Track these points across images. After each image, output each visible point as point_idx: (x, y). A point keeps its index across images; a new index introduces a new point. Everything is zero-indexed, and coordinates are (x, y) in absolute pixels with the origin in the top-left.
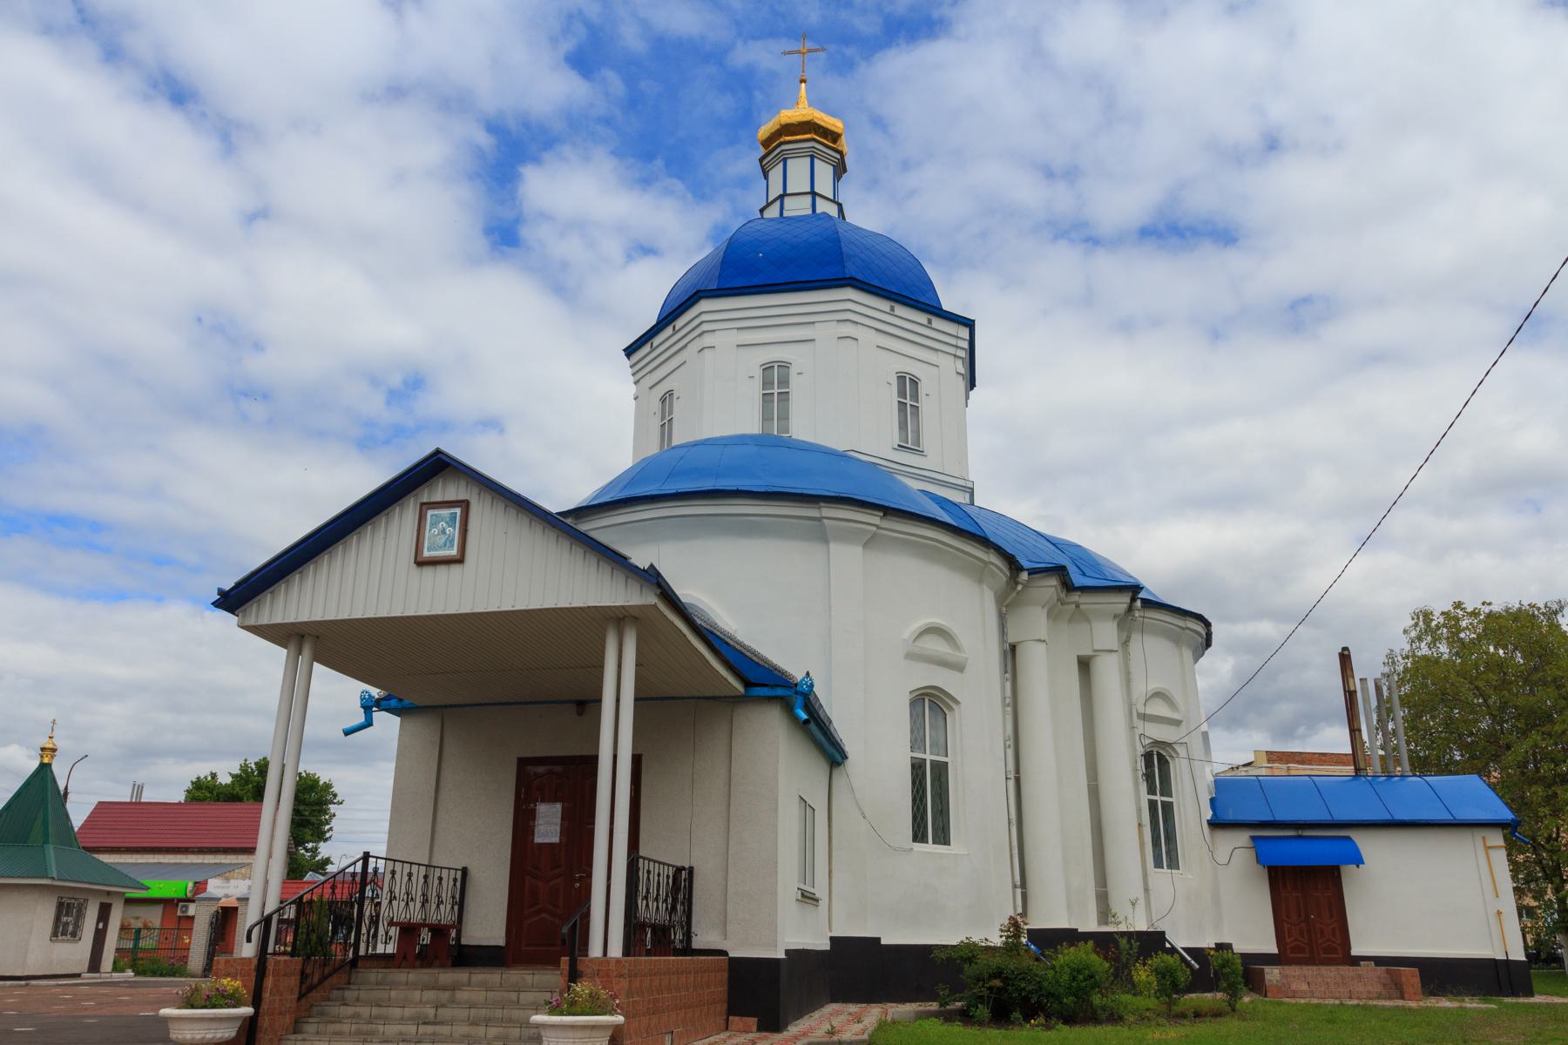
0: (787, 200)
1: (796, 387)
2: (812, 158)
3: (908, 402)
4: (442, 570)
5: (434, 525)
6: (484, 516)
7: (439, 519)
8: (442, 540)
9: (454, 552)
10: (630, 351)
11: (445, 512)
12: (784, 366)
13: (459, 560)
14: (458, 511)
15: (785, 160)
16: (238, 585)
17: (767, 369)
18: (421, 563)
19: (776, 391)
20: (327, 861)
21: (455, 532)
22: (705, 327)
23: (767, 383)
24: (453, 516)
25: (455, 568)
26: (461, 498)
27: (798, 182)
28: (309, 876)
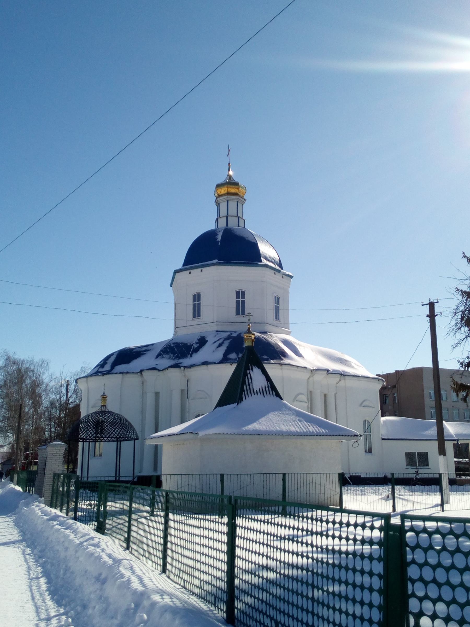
2: (228, 202)
3: (241, 300)
10: (171, 285)
12: (199, 295)
15: (219, 204)
17: (195, 296)
19: (241, 300)
23: (195, 301)
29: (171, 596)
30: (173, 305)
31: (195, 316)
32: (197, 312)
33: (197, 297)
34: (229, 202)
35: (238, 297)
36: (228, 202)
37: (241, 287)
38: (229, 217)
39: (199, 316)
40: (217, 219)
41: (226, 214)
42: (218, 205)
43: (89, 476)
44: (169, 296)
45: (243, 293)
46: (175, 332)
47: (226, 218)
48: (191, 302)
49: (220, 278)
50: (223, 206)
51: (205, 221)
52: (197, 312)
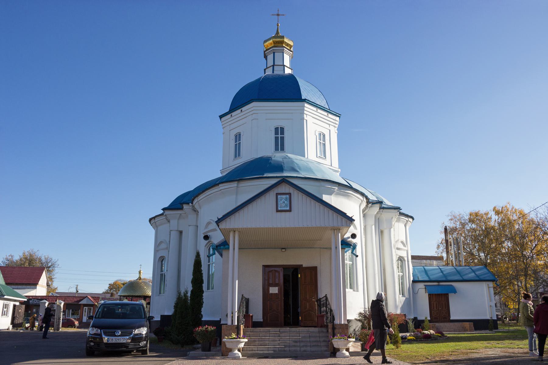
1: (286, 135)
2: (274, 53)
3: (279, 136)
4: (284, 213)
5: (281, 200)
6: (297, 197)
7: (282, 198)
8: (284, 205)
9: (288, 209)
11: (284, 196)
13: (290, 211)
14: (288, 196)
16: (193, 275)
18: (278, 211)
19: (279, 136)
20: (377, 305)
21: (287, 202)
22: (254, 112)
24: (286, 198)
25: (288, 213)
26: (287, 192)
27: (270, 63)
28: (420, 330)
33: (238, 137)
35: (276, 133)
36: (274, 53)
37: (279, 124)
39: (239, 155)
42: (266, 57)
45: (282, 129)
51: (256, 72)
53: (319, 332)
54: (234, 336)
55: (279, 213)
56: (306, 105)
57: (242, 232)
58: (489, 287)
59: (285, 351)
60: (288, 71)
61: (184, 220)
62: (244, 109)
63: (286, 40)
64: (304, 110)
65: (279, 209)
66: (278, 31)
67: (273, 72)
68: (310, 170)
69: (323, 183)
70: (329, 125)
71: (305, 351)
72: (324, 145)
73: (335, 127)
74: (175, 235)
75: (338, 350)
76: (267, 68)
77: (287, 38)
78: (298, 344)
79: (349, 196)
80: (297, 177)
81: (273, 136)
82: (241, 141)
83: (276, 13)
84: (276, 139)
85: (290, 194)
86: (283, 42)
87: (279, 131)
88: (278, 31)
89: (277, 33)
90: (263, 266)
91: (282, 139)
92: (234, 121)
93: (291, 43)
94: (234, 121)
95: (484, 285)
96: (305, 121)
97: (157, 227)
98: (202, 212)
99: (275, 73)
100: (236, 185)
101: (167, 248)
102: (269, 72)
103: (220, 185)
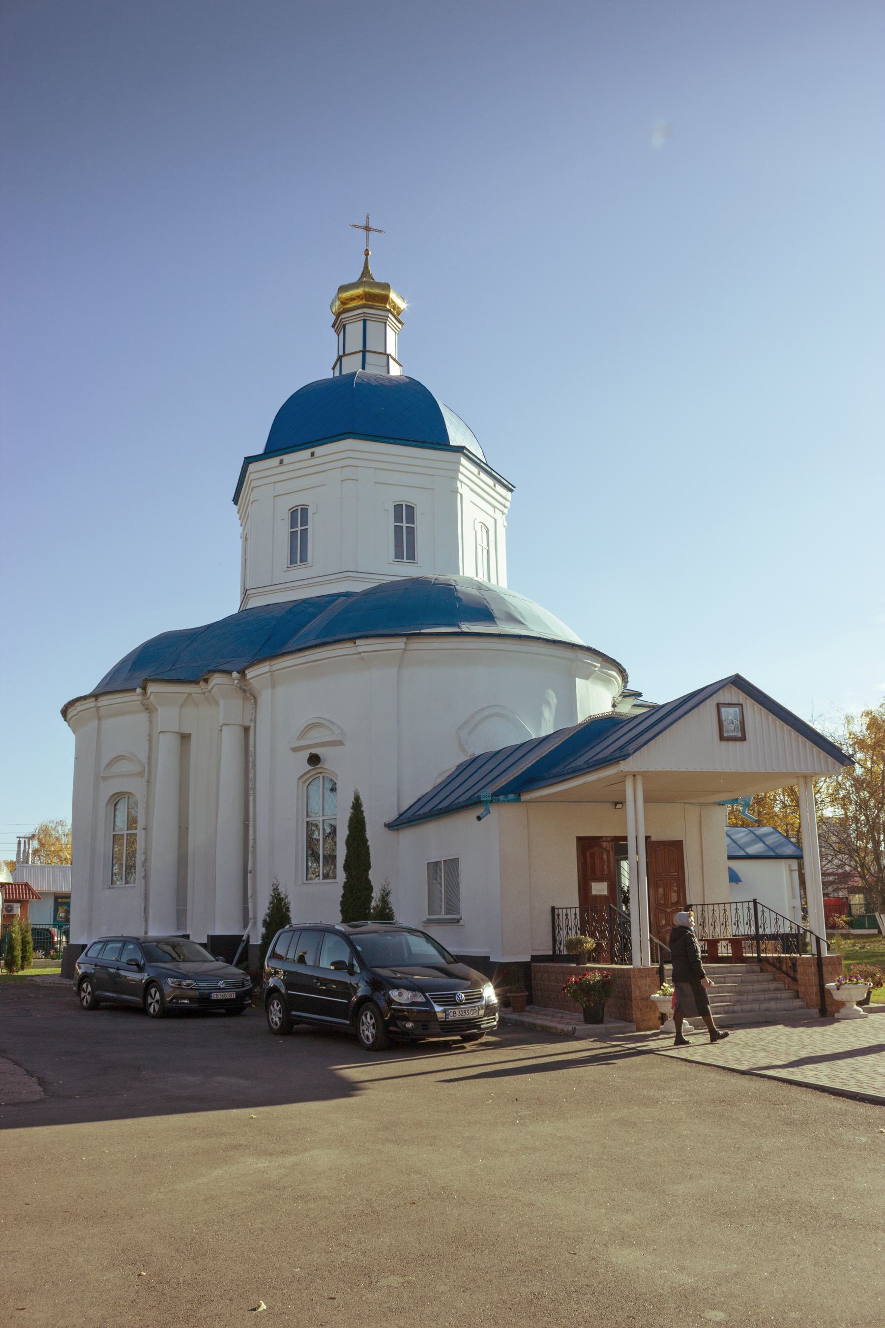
0: (344, 359)
2: (365, 321)
3: (404, 525)
10: (236, 500)
12: (305, 510)
15: (344, 326)
17: (293, 513)
23: (293, 524)
26: (735, 701)
27: (354, 342)
29: (808, 1069)
30: (239, 543)
31: (293, 561)
32: (298, 550)
33: (299, 516)
34: (368, 323)
35: (398, 517)
36: (365, 321)
37: (406, 497)
38: (368, 354)
39: (304, 559)
40: (340, 358)
41: (361, 348)
42: (339, 326)
43: (368, 348)
44: (229, 520)
45: (411, 509)
46: (245, 594)
47: (361, 354)
48: (284, 530)
49: (355, 474)
50: (354, 330)
51: (314, 361)
52: (298, 550)
53: (748, 972)
54: (170, 980)
55: (724, 743)
56: (463, 461)
57: (646, 776)
58: (791, 871)
59: (734, 1012)
60: (395, 370)
61: (208, 710)
62: (319, 450)
63: (393, 296)
64: (458, 471)
65: (725, 735)
66: (366, 267)
67: (363, 368)
68: (512, 619)
69: (581, 654)
70: (494, 507)
71: (767, 1010)
72: (488, 551)
73: (503, 514)
74: (167, 746)
75: (842, 1004)
76: (345, 355)
77: (396, 291)
78: (744, 998)
79: (611, 681)
80: (520, 637)
81: (391, 524)
82: (310, 527)
83: (363, 223)
84: (398, 530)
85: (741, 705)
86: (385, 299)
87: (404, 513)
88: (366, 267)
89: (366, 272)
90: (580, 839)
91: (411, 531)
92: (288, 476)
93: (402, 305)
94: (288, 476)
95: (783, 865)
96: (459, 495)
97: (99, 719)
98: (265, 697)
99: (369, 370)
100: (402, 645)
101: (141, 774)
102: (352, 365)
103: (358, 642)
